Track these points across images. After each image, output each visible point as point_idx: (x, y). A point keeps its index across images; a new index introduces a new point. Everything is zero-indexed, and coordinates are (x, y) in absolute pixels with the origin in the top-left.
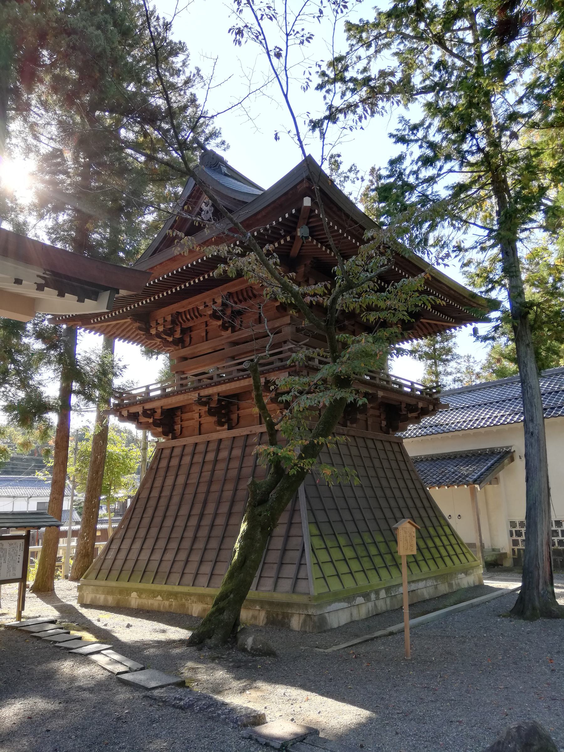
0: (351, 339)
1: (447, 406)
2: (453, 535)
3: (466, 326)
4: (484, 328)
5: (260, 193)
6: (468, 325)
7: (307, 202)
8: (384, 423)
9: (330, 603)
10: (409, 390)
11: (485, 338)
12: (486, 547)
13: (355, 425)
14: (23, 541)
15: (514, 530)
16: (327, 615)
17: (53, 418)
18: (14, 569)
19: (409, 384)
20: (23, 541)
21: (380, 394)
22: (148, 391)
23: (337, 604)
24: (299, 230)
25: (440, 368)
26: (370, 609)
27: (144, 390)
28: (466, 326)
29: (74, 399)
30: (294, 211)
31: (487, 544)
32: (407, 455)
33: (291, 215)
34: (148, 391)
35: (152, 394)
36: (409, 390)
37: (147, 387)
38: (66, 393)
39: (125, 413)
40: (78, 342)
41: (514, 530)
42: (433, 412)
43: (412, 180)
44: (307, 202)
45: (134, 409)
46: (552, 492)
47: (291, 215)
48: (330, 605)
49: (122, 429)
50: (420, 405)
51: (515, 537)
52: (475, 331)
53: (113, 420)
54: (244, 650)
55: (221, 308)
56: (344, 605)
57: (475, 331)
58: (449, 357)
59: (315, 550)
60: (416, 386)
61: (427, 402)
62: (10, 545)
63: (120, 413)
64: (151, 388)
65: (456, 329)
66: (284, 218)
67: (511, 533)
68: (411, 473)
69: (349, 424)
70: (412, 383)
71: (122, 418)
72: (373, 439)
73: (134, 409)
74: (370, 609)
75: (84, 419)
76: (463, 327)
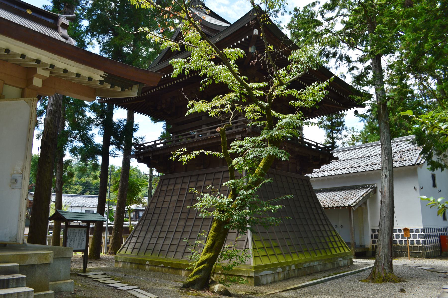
0: (281, 116)
1: (337, 158)
2: (323, 214)
3: (351, 109)
4: (361, 111)
5: (228, 25)
6: (352, 108)
7: (256, 32)
8: (298, 168)
9: (262, 271)
10: (315, 148)
11: (361, 116)
12: (357, 244)
13: (281, 168)
14: (86, 229)
15: (374, 234)
16: (260, 277)
17: (100, 159)
18: (81, 244)
19: (315, 144)
20: (86, 229)
21: (297, 149)
22: (155, 144)
23: (266, 271)
24: (250, 48)
25: (335, 135)
26: (286, 275)
27: (153, 143)
28: (351, 109)
29: (111, 148)
30: (247, 37)
31: (358, 243)
32: (312, 188)
33: (245, 39)
34: (155, 144)
35: (158, 146)
36: (315, 148)
37: (155, 142)
38: (107, 142)
39: (142, 157)
40: (114, 112)
41: (374, 234)
42: (328, 162)
43: (319, 18)
44: (256, 32)
45: (148, 155)
46: (395, 209)
47: (245, 39)
48: (262, 272)
49: (140, 168)
50: (321, 157)
51: (374, 239)
52: (356, 112)
53: (134, 163)
54: (213, 292)
55: (95, 117)
56: (271, 272)
57: (356, 112)
58: (340, 128)
59: (255, 241)
60: (319, 145)
61: (325, 155)
62: (79, 230)
63: (139, 157)
64: (157, 142)
65: (344, 111)
66: (241, 41)
67: (372, 236)
68: (314, 198)
69: (277, 167)
70: (317, 143)
71: (140, 161)
72: (291, 177)
73: (148, 155)
74: (286, 275)
75: (116, 162)
76: (349, 109)
